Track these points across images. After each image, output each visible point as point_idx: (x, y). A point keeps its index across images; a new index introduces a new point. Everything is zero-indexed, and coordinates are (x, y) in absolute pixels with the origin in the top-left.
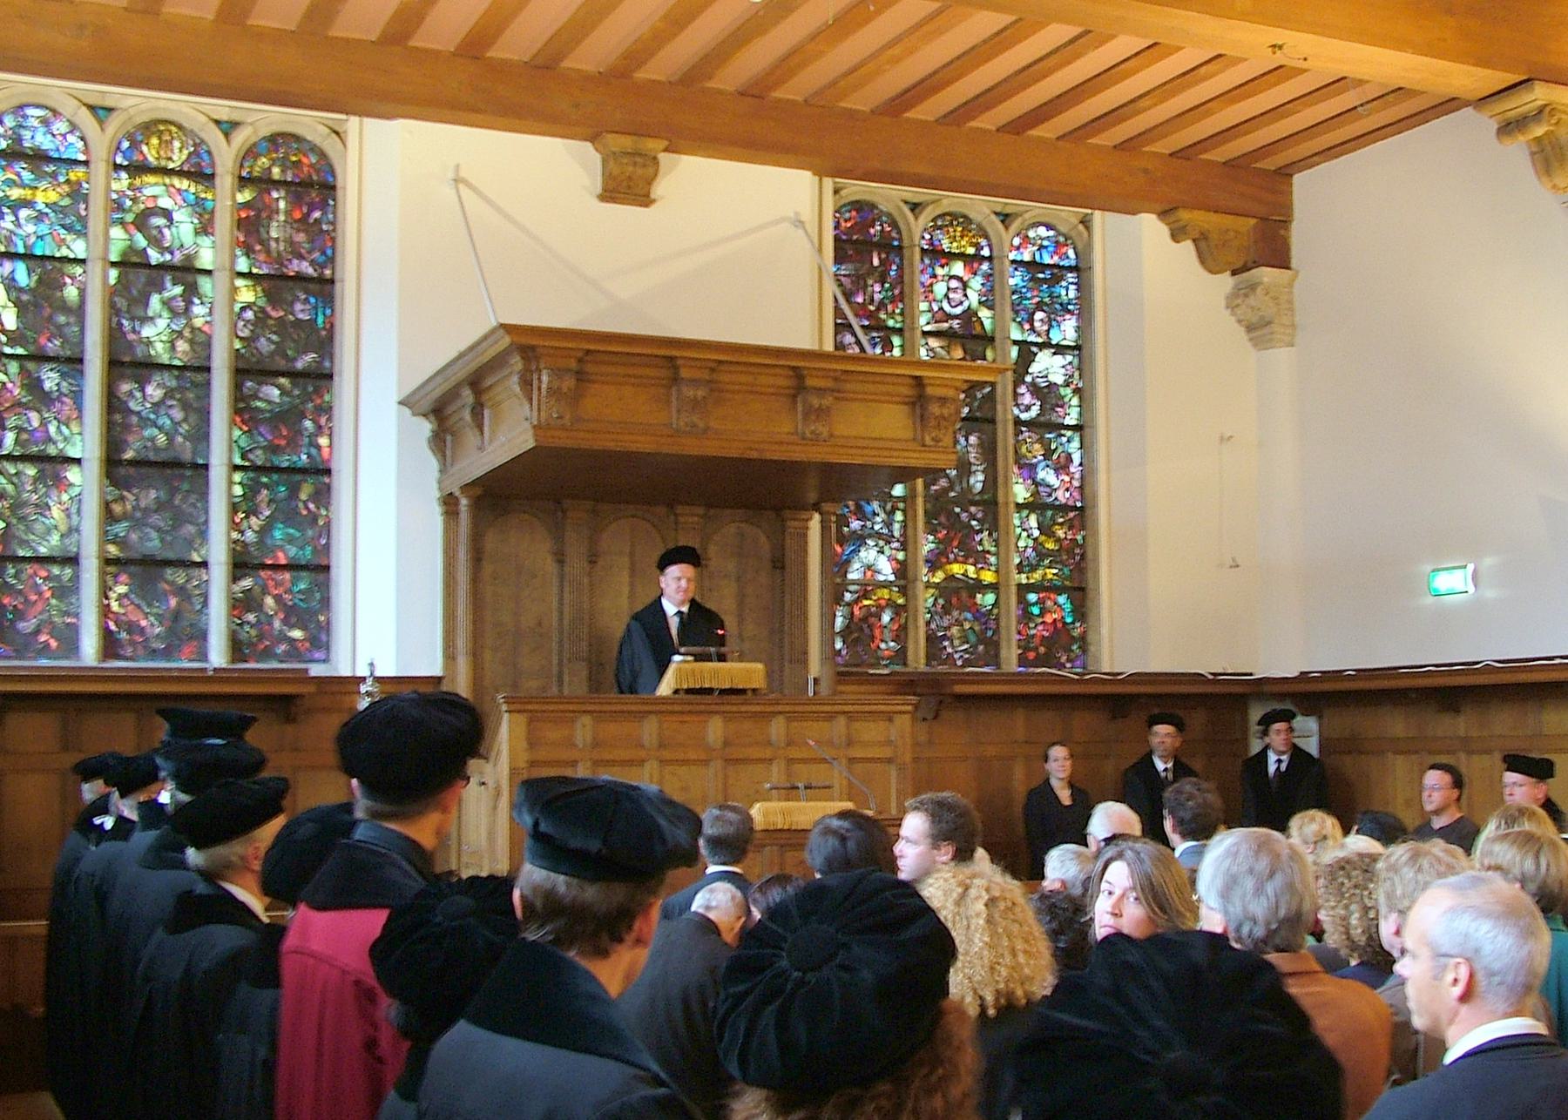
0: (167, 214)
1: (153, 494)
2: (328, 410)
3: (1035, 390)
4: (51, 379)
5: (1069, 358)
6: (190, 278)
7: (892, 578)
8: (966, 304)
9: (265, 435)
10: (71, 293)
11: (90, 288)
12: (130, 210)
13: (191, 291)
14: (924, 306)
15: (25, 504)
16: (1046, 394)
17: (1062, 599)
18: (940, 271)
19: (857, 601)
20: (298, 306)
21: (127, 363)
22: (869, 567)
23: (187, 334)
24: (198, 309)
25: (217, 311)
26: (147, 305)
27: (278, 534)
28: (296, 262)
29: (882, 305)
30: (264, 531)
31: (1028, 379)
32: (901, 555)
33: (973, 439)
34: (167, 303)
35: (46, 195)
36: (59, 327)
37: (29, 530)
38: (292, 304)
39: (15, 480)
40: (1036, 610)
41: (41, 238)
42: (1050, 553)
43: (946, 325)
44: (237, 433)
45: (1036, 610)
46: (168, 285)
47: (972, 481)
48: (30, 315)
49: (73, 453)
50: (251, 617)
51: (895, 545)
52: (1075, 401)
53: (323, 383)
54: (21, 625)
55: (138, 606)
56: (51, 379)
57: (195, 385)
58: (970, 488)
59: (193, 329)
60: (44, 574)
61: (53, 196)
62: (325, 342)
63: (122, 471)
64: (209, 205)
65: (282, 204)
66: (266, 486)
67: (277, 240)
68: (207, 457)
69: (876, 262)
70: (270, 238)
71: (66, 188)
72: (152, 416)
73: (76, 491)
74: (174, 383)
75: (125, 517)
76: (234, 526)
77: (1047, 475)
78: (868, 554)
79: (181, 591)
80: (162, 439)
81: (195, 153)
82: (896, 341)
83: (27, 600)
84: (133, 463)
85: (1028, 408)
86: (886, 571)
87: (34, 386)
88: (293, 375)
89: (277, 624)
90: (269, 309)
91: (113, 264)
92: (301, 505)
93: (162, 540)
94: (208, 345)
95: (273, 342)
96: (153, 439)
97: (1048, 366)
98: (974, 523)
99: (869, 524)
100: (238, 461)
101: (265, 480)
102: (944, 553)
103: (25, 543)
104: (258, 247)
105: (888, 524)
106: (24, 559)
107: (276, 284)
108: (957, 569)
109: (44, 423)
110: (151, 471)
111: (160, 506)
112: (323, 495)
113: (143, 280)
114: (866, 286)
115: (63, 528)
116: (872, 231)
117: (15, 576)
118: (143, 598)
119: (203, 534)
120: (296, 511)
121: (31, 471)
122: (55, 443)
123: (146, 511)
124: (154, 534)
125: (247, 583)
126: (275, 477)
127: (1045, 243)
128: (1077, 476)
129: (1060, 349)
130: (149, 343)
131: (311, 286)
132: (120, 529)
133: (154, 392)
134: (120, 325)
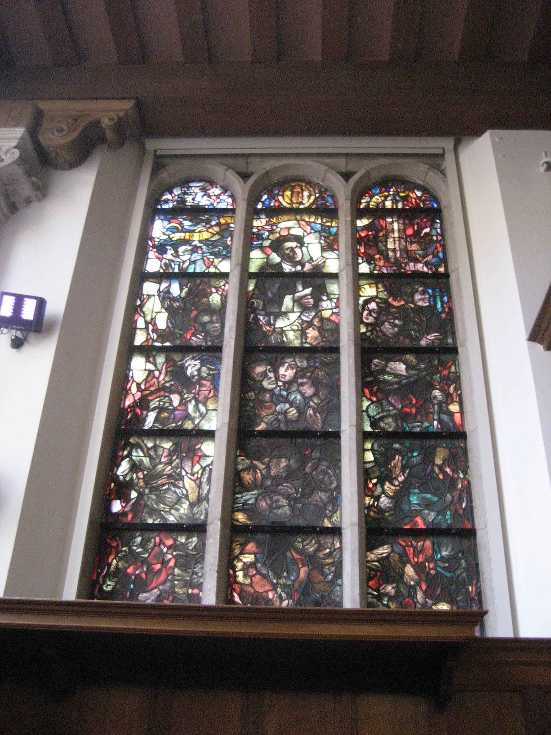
0: (299, 240)
1: (283, 463)
2: (457, 380)
4: (192, 366)
6: (318, 281)
9: (395, 403)
10: (215, 299)
11: (225, 296)
12: (268, 238)
13: (320, 292)
15: (160, 475)
20: (417, 297)
21: (257, 348)
23: (316, 322)
24: (326, 304)
25: (343, 304)
26: (281, 304)
27: (414, 499)
28: (412, 264)
30: (399, 497)
34: (298, 302)
35: (201, 234)
36: (204, 324)
37: (161, 499)
38: (412, 295)
39: (152, 453)
41: (194, 262)
44: (366, 403)
46: (300, 288)
48: (179, 318)
49: (206, 426)
50: (390, 589)
53: (445, 357)
54: (143, 596)
55: (264, 576)
56: (192, 366)
57: (325, 365)
59: (322, 319)
60: (170, 542)
61: (206, 235)
62: (447, 323)
63: (254, 442)
64: (334, 230)
65: (396, 226)
66: (398, 452)
67: (394, 250)
68: (473, 524)
70: (387, 249)
71: (217, 229)
72: (284, 393)
73: (208, 461)
74: (305, 364)
75: (255, 485)
76: (364, 490)
79: (312, 560)
80: (293, 412)
81: (322, 197)
83: (150, 569)
84: (264, 434)
87: (177, 373)
88: (418, 351)
89: (420, 596)
90: (390, 300)
91: (252, 276)
92: (437, 470)
93: (292, 508)
94: (336, 330)
95: (396, 326)
96: (285, 413)
100: (368, 428)
101: (397, 446)
103: (153, 512)
104: (377, 256)
106: (154, 528)
107: (395, 280)
109: (184, 403)
110: (282, 440)
111: (291, 475)
112: (460, 459)
113: (277, 285)
115: (193, 497)
117: (140, 545)
118: (271, 567)
119: (335, 500)
120: (432, 476)
121: (167, 445)
122: (193, 420)
123: (278, 480)
124: (283, 502)
125: (384, 550)
126: (407, 443)
130: (282, 332)
131: (428, 281)
132: (249, 497)
133: (286, 372)
134: (257, 320)
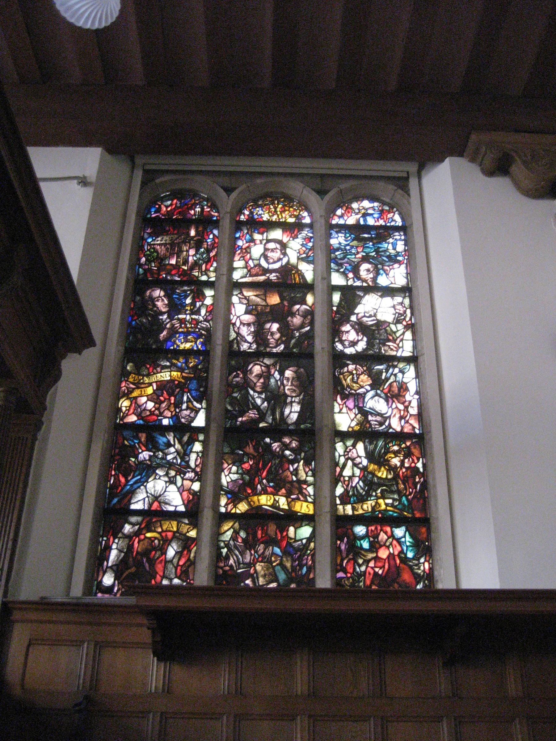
3: (361, 328)
5: (399, 299)
7: (182, 509)
8: (285, 260)
14: (241, 264)
16: (374, 332)
17: (399, 532)
18: (257, 237)
19: (137, 534)
22: (156, 498)
29: (196, 264)
31: (353, 318)
32: (196, 486)
33: (288, 373)
40: (366, 545)
42: (382, 482)
43: (262, 278)
45: (366, 545)
47: (287, 411)
51: (190, 475)
52: (408, 335)
58: (283, 419)
69: (193, 233)
77: (376, 403)
78: (156, 485)
82: (209, 293)
85: (354, 344)
86: (175, 501)
97: (372, 307)
98: (287, 452)
99: (160, 454)
102: (251, 484)
105: (184, 454)
108: (265, 500)
114: (180, 251)
116: (192, 212)
127: (370, 211)
128: (414, 404)
129: (388, 291)
